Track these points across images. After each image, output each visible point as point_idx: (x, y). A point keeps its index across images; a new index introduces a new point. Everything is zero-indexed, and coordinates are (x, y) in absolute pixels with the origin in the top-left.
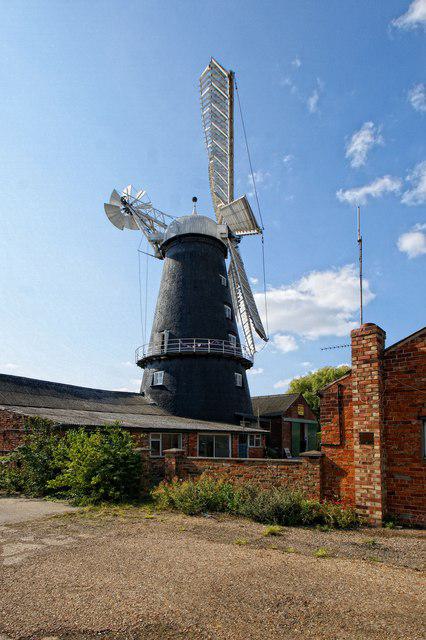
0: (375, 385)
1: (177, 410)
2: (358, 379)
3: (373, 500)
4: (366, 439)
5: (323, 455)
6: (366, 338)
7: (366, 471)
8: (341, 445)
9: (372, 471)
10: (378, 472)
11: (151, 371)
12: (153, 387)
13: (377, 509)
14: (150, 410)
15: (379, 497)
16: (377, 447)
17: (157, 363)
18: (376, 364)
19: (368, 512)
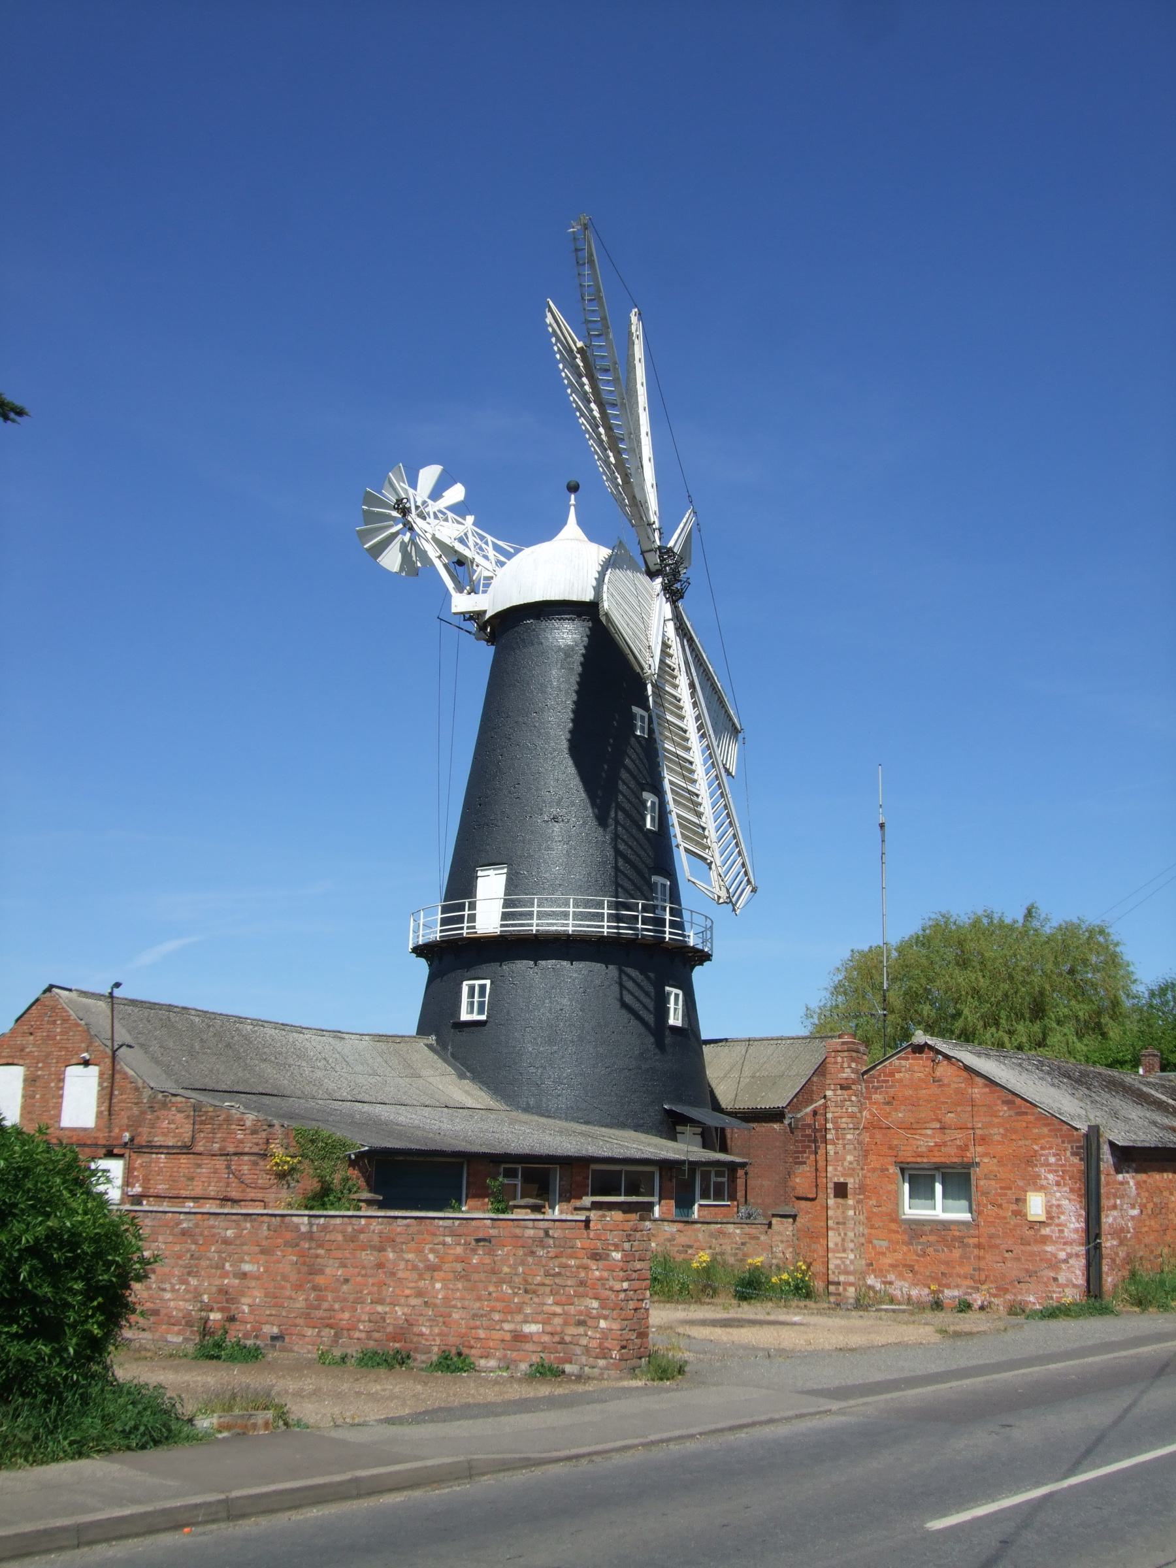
13: (851, 1284)
19: (841, 1288)
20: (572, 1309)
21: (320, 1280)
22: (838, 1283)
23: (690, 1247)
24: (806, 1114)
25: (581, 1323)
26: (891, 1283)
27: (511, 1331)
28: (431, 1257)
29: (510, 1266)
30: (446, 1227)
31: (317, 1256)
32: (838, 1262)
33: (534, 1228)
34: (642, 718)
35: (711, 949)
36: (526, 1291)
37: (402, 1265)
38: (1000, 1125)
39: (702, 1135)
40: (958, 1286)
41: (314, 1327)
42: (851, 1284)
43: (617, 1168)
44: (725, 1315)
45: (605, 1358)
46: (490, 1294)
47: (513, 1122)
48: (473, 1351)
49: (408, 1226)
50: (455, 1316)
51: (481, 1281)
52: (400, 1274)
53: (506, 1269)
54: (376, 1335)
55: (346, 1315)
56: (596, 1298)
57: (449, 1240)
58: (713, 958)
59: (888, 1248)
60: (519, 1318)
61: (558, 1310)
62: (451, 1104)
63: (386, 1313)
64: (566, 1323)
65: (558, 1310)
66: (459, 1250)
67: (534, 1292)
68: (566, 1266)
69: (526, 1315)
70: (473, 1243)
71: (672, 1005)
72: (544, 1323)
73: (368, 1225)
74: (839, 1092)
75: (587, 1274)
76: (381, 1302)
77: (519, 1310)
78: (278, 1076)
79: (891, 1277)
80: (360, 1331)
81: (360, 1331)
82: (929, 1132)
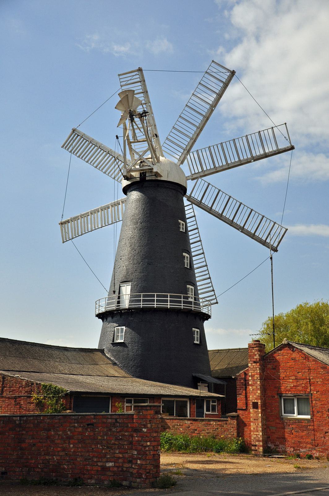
0: (258, 376)
1: (142, 372)
2: (251, 371)
3: (259, 441)
4: (255, 406)
5: (238, 416)
6: (254, 349)
7: (255, 424)
8: (246, 410)
9: (258, 424)
10: (260, 424)
11: (113, 326)
12: (114, 344)
13: (261, 446)
14: (112, 371)
15: (261, 439)
16: (260, 410)
17: (118, 317)
18: (258, 364)
19: (257, 448)
20: (126, 455)
21: (23, 445)
22: (256, 446)
23: (196, 430)
24: (241, 373)
25: (130, 462)
26: (278, 446)
27: (101, 466)
28: (69, 433)
29: (101, 436)
30: (75, 419)
31: (22, 434)
32: (255, 436)
33: (111, 418)
34: (183, 224)
35: (211, 314)
36: (108, 447)
37: (57, 437)
38: (321, 378)
39: (208, 387)
40: (305, 447)
41: (20, 467)
42: (261, 446)
43: (173, 399)
44: (207, 459)
45: (139, 478)
46: (93, 449)
47: (132, 382)
48: (85, 476)
49: (59, 419)
50: (78, 460)
51: (89, 443)
52: (56, 441)
53: (99, 438)
54: (45, 470)
55: (33, 461)
56: (136, 450)
57: (76, 425)
58: (212, 317)
59: (276, 430)
60: (104, 460)
61: (121, 456)
62: (109, 375)
63: (50, 459)
64: (124, 462)
65: (121, 456)
66: (80, 429)
67: (111, 447)
68: (124, 435)
69: (108, 458)
70: (86, 426)
71: (196, 336)
72: (114, 462)
73: (43, 419)
74: (254, 364)
75: (132, 439)
76: (48, 454)
77: (105, 456)
78: (40, 365)
79: (278, 443)
80: (39, 468)
81: (39, 468)
82: (291, 381)
